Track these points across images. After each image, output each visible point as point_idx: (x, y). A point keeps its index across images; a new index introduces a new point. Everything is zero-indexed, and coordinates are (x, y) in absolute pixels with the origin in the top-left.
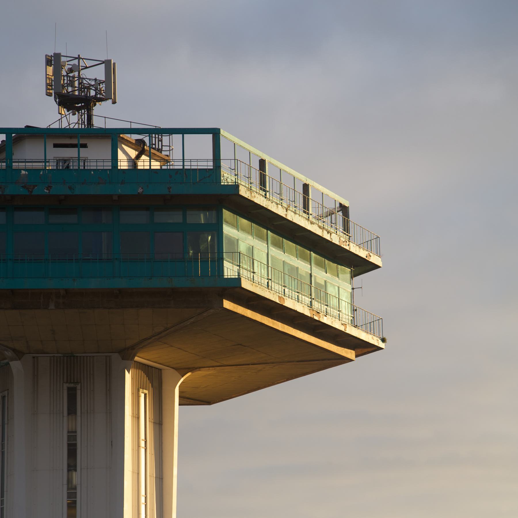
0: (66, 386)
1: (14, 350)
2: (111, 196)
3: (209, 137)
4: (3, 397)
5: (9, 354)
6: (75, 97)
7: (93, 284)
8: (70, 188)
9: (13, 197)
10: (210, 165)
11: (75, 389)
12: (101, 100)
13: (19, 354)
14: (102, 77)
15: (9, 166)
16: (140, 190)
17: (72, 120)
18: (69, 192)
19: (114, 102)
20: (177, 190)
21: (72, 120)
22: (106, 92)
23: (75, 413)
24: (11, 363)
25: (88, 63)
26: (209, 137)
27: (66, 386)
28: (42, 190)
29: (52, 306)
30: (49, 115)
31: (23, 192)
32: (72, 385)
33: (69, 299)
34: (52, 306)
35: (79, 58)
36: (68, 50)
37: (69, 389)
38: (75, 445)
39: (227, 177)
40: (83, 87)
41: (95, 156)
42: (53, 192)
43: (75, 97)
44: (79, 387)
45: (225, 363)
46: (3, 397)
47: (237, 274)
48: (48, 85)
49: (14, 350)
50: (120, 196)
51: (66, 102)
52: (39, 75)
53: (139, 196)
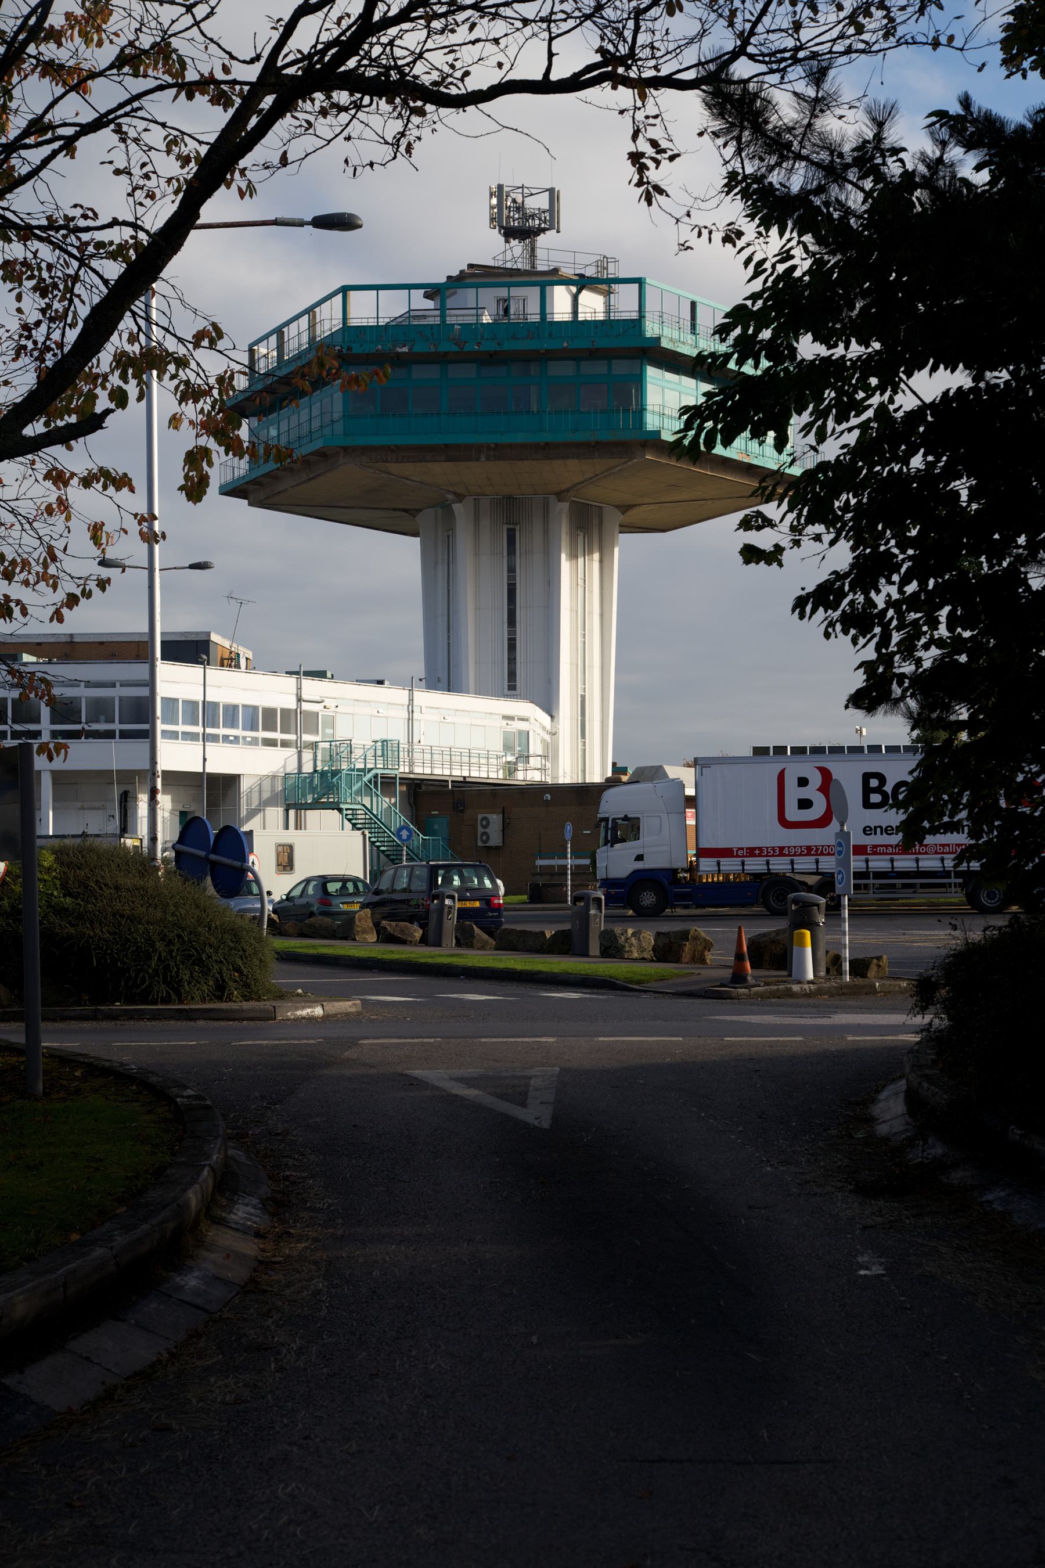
0: (505, 527)
1: (455, 494)
2: (538, 351)
3: (637, 285)
4: (448, 537)
5: (450, 497)
6: (520, 227)
7: (520, 438)
8: (499, 344)
9: (446, 353)
10: (635, 316)
11: (514, 530)
12: (544, 230)
13: (460, 497)
14: (546, 206)
15: (443, 321)
16: (565, 345)
17: (515, 253)
18: (498, 349)
19: (558, 232)
20: (602, 343)
21: (515, 253)
22: (551, 220)
23: (515, 554)
24: (453, 505)
25: (534, 191)
26: (637, 285)
27: (505, 527)
28: (472, 347)
29: (483, 459)
30: (491, 248)
31: (456, 349)
32: (511, 526)
33: (500, 452)
34: (483, 459)
35: (522, 187)
36: (508, 182)
37: (508, 530)
38: (515, 584)
39: (651, 329)
40: (526, 217)
41: (526, 303)
42: (482, 349)
43: (520, 227)
44: (518, 528)
45: (663, 500)
46: (448, 537)
47: (286, 859)
48: (492, 220)
49: (455, 494)
50: (547, 350)
51: (509, 233)
52: (483, 206)
53: (565, 349)
